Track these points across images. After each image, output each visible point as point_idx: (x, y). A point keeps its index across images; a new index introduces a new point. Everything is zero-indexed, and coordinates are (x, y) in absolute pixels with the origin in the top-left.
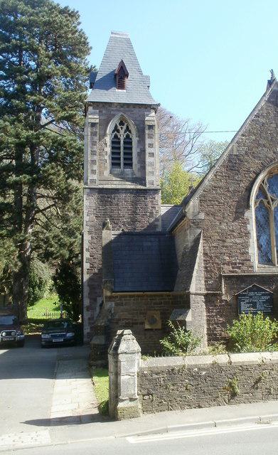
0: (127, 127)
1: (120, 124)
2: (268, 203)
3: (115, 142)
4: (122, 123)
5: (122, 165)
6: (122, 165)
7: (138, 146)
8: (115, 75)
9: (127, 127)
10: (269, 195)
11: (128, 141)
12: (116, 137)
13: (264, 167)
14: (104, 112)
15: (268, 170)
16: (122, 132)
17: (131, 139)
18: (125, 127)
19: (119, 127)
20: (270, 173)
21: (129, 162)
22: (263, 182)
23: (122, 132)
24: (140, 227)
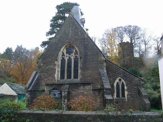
20: (65, 47)
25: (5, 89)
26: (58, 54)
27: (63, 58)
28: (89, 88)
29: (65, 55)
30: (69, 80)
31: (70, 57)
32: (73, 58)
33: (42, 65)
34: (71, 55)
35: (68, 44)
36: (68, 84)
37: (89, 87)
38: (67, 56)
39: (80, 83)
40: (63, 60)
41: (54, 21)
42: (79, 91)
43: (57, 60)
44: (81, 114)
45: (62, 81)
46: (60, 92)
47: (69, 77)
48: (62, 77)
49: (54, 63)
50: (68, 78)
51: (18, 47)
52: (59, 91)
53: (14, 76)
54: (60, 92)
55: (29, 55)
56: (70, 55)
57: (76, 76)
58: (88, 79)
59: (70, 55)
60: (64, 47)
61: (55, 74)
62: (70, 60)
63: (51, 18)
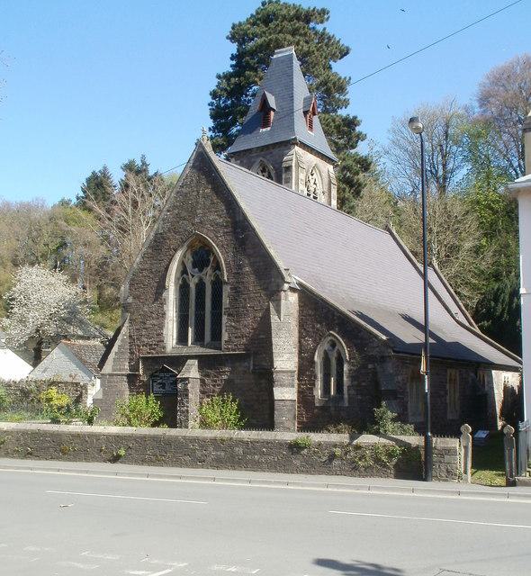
26: (169, 265)
27: (184, 280)
29: (189, 271)
32: (208, 280)
33: (130, 300)
34: (204, 272)
36: (426, 323)
37: (246, 364)
38: (193, 276)
41: (230, 94)
44: (156, 433)
45: (185, 351)
47: (199, 339)
48: (182, 339)
51: (355, 118)
53: (285, 291)
56: (201, 271)
59: (201, 271)
62: (201, 287)
63: (213, 84)
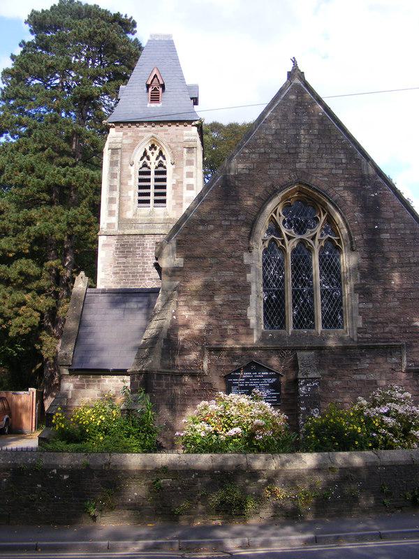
0: (161, 153)
1: (150, 149)
2: (283, 242)
3: (144, 173)
4: (153, 147)
5: (152, 201)
6: (152, 201)
7: (173, 176)
8: (236, 134)
9: (161, 153)
10: (284, 231)
11: (161, 172)
12: (145, 165)
13: (274, 193)
14: (129, 134)
15: (281, 195)
16: (153, 158)
17: (165, 167)
18: (157, 153)
19: (149, 153)
20: (285, 198)
21: (162, 198)
22: (275, 213)
23: (153, 158)
24: (20, 410)
25: (3, 140)
28: (394, 367)
30: (153, 105)
31: (302, 242)
35: (296, 190)
37: (394, 359)
39: (361, 348)
40: (273, 248)
42: (358, 377)
43: (249, 249)
46: (274, 380)
49: (240, 262)
50: (298, 324)
52: (271, 377)
54: (274, 380)
55: (247, 481)
57: (332, 321)
58: (387, 330)
60: (276, 200)
61: (249, 304)
62: (302, 254)
